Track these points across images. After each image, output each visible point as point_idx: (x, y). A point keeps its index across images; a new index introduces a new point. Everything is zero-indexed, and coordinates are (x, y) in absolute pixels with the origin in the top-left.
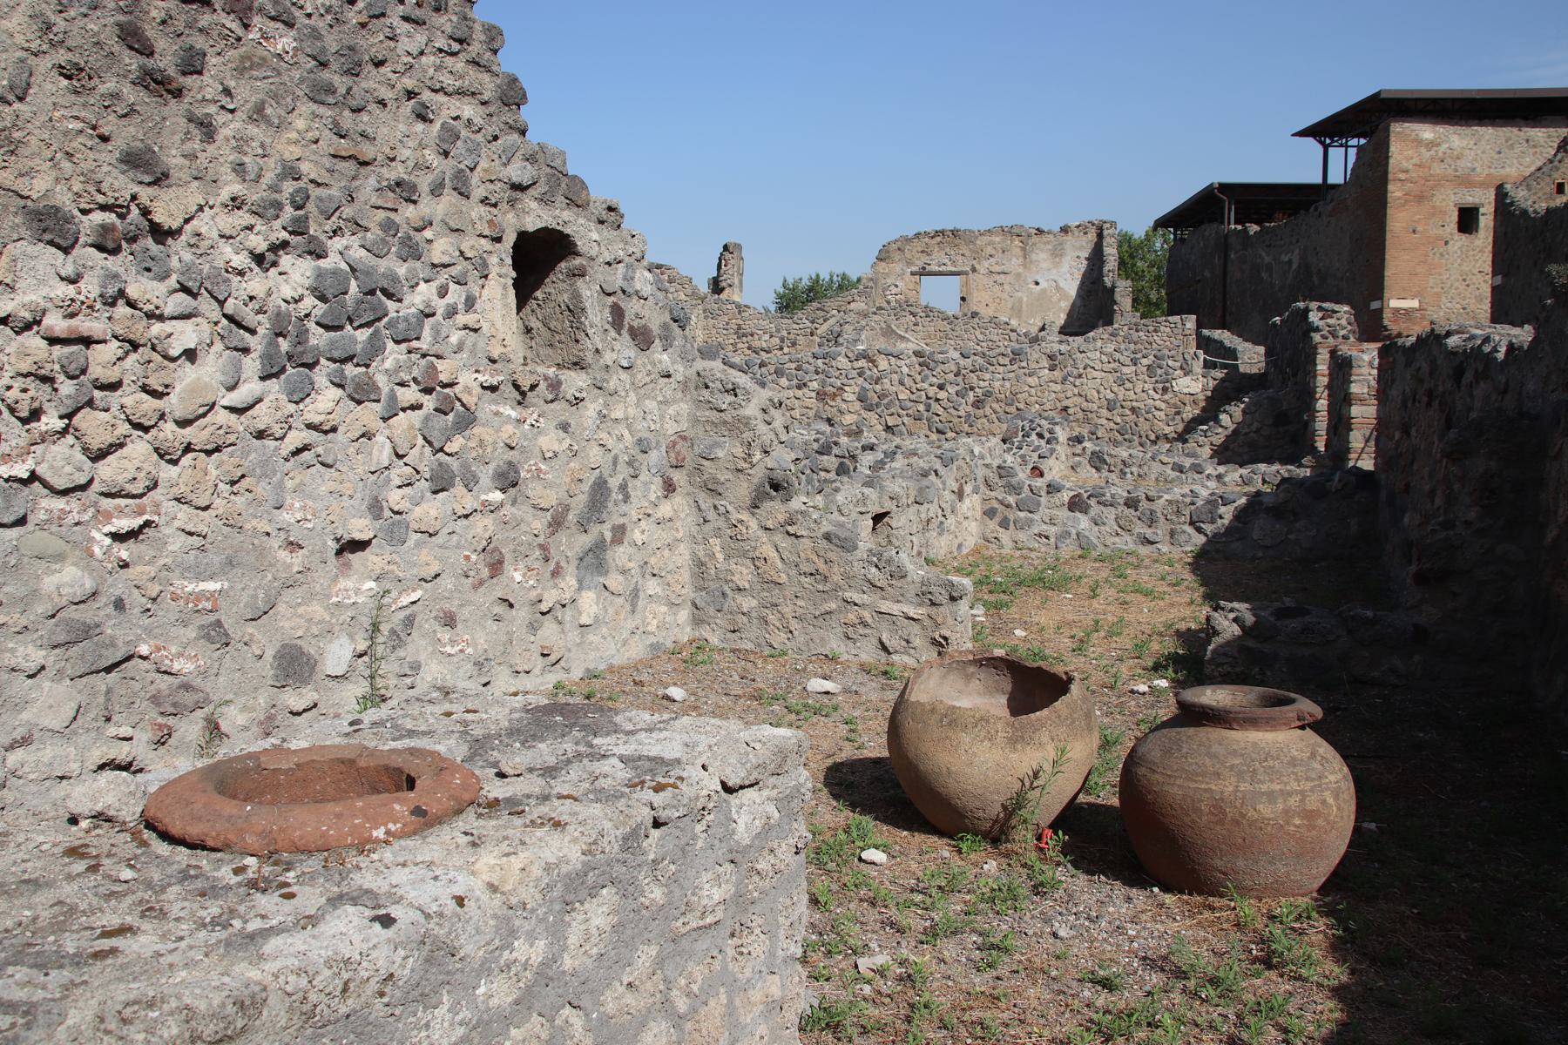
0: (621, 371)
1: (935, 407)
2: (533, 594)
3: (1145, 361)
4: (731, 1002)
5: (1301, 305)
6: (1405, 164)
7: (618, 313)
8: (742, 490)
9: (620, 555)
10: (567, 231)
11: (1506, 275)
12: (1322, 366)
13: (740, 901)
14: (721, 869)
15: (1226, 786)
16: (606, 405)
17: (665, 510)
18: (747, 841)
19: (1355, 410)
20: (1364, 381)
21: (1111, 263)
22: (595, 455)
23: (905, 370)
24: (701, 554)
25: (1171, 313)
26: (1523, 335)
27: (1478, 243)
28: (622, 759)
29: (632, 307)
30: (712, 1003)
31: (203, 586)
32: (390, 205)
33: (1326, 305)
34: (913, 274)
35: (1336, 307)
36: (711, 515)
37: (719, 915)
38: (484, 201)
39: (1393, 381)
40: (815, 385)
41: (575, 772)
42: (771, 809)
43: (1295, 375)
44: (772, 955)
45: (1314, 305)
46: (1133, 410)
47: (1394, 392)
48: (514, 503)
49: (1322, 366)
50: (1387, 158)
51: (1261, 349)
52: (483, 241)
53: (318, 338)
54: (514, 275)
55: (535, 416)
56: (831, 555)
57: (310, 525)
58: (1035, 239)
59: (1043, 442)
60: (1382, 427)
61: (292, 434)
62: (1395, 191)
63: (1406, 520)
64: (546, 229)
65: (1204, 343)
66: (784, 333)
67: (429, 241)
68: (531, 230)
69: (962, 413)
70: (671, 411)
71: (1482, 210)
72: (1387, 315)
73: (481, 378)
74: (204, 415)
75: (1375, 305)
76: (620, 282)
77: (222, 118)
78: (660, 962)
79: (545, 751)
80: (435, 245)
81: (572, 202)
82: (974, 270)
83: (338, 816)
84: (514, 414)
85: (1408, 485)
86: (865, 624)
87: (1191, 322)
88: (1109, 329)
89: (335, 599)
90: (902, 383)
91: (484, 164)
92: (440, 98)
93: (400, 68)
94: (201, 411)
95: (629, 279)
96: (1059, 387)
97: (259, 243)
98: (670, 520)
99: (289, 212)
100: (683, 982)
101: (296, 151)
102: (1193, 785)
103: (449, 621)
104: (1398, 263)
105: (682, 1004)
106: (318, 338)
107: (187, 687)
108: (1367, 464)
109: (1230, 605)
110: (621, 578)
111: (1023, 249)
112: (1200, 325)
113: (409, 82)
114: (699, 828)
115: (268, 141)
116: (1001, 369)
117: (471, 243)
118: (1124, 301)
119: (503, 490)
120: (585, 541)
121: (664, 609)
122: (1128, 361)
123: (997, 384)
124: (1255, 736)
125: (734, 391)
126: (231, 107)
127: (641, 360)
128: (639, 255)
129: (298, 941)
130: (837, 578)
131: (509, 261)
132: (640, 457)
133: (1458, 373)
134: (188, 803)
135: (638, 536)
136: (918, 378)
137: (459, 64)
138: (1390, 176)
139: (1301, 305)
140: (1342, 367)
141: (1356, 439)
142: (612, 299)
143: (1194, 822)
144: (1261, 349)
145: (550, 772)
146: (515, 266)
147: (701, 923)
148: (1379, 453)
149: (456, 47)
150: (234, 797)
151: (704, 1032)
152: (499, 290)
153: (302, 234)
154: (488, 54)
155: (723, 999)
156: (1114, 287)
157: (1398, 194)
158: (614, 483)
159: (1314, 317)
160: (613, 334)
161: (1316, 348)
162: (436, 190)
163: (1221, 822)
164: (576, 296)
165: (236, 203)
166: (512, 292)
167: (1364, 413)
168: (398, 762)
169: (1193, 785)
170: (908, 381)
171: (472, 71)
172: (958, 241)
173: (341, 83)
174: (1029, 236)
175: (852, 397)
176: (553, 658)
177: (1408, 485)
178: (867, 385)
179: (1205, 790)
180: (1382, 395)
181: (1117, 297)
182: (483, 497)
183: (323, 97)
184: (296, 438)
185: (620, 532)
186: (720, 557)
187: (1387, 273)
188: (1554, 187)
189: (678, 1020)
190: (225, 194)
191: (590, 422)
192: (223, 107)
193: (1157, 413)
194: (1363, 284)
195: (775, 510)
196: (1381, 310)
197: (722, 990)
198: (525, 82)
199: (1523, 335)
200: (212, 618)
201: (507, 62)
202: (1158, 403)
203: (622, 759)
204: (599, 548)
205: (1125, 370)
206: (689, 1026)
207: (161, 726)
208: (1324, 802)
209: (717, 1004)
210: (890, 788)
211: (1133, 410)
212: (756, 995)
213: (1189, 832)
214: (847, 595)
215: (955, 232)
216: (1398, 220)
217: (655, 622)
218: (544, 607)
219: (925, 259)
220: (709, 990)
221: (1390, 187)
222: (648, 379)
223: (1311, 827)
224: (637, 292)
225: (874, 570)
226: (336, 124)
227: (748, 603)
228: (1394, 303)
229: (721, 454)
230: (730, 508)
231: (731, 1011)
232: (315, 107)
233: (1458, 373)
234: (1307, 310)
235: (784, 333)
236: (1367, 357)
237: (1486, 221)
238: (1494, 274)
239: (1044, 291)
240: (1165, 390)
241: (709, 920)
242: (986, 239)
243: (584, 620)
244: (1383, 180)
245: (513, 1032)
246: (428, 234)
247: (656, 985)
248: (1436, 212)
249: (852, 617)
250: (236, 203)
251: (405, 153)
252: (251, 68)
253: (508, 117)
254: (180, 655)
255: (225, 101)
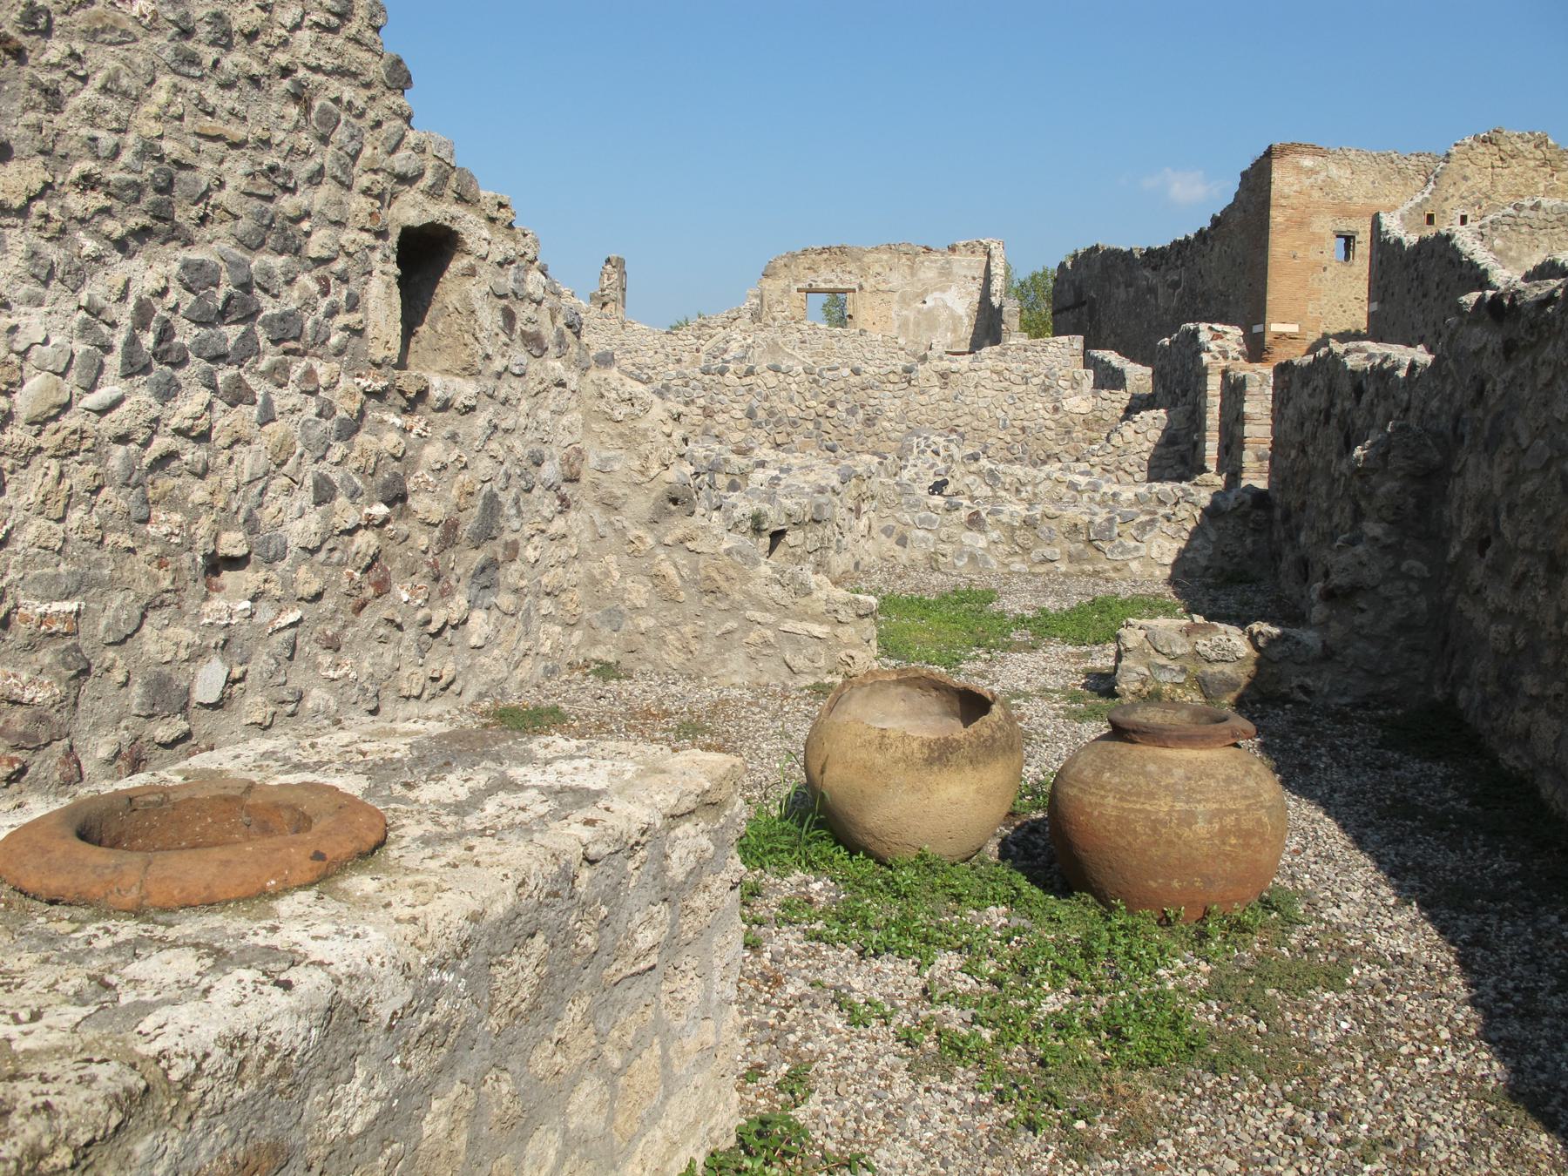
0: (513, 378)
1: (826, 425)
2: (420, 615)
3: (1036, 381)
4: (665, 1051)
5: (1191, 326)
6: (1286, 190)
7: (509, 317)
8: (641, 504)
9: (511, 574)
10: (456, 227)
11: (1382, 302)
12: (1214, 384)
13: (672, 945)
14: (655, 909)
15: (1162, 806)
16: (497, 414)
17: (558, 525)
18: (681, 878)
19: (1248, 429)
20: (1258, 405)
21: (997, 284)
22: (484, 466)
23: (794, 387)
24: (596, 572)
25: (1056, 333)
26: (1410, 356)
27: (1355, 270)
28: (542, 790)
29: (524, 311)
30: (645, 1054)
31: (56, 606)
32: (264, 192)
33: (1217, 326)
34: (799, 290)
35: (1227, 328)
36: (608, 531)
37: (653, 959)
38: (366, 192)
39: (1289, 399)
40: (701, 402)
41: (491, 807)
42: (704, 841)
43: (1185, 395)
44: (708, 1000)
45: (1203, 326)
46: (1023, 429)
47: (1290, 411)
48: (400, 516)
49: (1214, 384)
50: (1270, 183)
51: (1149, 371)
52: (365, 236)
53: (186, 333)
54: (398, 272)
55: (422, 424)
56: (732, 573)
57: (178, 540)
58: (922, 257)
59: (938, 461)
60: (1279, 445)
61: (157, 441)
62: (1277, 217)
63: (1302, 538)
64: (432, 224)
65: (1089, 362)
66: (669, 349)
67: (308, 234)
68: (417, 225)
69: (852, 432)
70: (565, 421)
71: (1358, 238)
72: (1268, 339)
73: (364, 383)
74: (56, 418)
75: (1257, 329)
76: (511, 285)
77: (68, 86)
78: (590, 1017)
79: (453, 786)
80: (313, 237)
81: (461, 199)
82: (861, 288)
83: (226, 863)
84: (398, 422)
85: (1304, 503)
86: (767, 644)
87: (1078, 342)
88: (997, 348)
89: (206, 621)
90: (791, 400)
91: (367, 151)
92: (319, 78)
93: (274, 41)
94: (53, 412)
95: (520, 281)
96: (949, 406)
97: (115, 228)
98: (564, 536)
99: (150, 196)
100: (615, 1034)
101: (155, 128)
102: (1126, 805)
103: (333, 645)
104: (1279, 289)
105: (616, 1061)
106: (186, 333)
107: (41, 719)
108: (1262, 484)
109: (1140, 622)
110: (512, 597)
111: (911, 267)
112: (1087, 346)
113: (282, 58)
114: (631, 865)
115: (124, 114)
116: (890, 387)
117: (352, 236)
118: (1012, 321)
119: (389, 504)
120: (478, 557)
121: (558, 629)
122: (1019, 380)
123: (887, 402)
124: (1188, 753)
125: (630, 400)
126: (81, 73)
127: (534, 366)
128: (530, 256)
129: (184, 1014)
130: (738, 597)
131: (394, 257)
132: (533, 469)
133: (1359, 391)
134: (45, 852)
135: (530, 553)
136: (808, 395)
137: (337, 41)
138: (1273, 202)
139: (1191, 326)
140: (1234, 390)
141: (1248, 458)
142: (505, 302)
143: (1129, 844)
144: (1149, 371)
145: (460, 809)
146: (400, 263)
147: (634, 969)
148: (1274, 471)
149: (334, 21)
150: (100, 843)
151: (638, 1087)
152: (383, 288)
153: (165, 220)
154: (369, 33)
155: (657, 1050)
156: (1001, 306)
157: (1280, 219)
158: (506, 498)
159: (1204, 337)
160: (503, 338)
161: (1206, 368)
162: (316, 178)
163: (1156, 843)
164: (466, 299)
165: (88, 182)
166: (396, 290)
167: (1258, 431)
168: (291, 798)
169: (1126, 805)
170: (798, 399)
171: (351, 48)
172: (844, 258)
173: (209, 55)
174: (917, 254)
175: (739, 415)
176: (442, 683)
177: (1304, 503)
178: (755, 404)
179: (1140, 811)
180: (1278, 415)
181: (1005, 317)
182: (367, 510)
183: (185, 69)
184: (160, 445)
185: (513, 550)
186: (617, 575)
187: (1269, 297)
188: (1424, 218)
189: (611, 1077)
190: (76, 171)
191: (480, 431)
192: (71, 74)
193: (1048, 433)
194: (1246, 304)
195: (679, 527)
196: (1263, 334)
197: (656, 1040)
198: (409, 64)
199: (1410, 356)
200: (69, 642)
201: (393, 42)
202: (1049, 423)
203: (542, 790)
204: (491, 565)
205: (1015, 389)
206: (622, 1081)
207: (11, 761)
208: (1259, 821)
209: (652, 1055)
210: (818, 821)
211: (1023, 429)
212: (691, 1044)
213: (1123, 855)
214: (748, 614)
215: (842, 249)
216: (1280, 246)
217: (549, 643)
218: (433, 628)
219: (812, 275)
220: (641, 1041)
221: (1273, 213)
222: (541, 387)
223: (1247, 846)
224: (529, 295)
225: (778, 587)
226: (201, 99)
227: (646, 623)
228: (1275, 328)
229: (617, 467)
230: (626, 524)
231: (666, 1062)
232: (177, 79)
233: (1359, 391)
234: (1196, 332)
235: (669, 349)
236: (1260, 381)
237: (1363, 247)
238: (1370, 300)
239: (930, 310)
240: (1056, 409)
241: (643, 965)
242: (875, 256)
243: (474, 641)
244: (1265, 205)
245: (435, 1105)
246: (305, 226)
247: (587, 1040)
248: (1316, 239)
249: (753, 637)
250: (88, 182)
251: (279, 136)
252: (103, 31)
253: (393, 100)
254: (31, 681)
255: (73, 66)
